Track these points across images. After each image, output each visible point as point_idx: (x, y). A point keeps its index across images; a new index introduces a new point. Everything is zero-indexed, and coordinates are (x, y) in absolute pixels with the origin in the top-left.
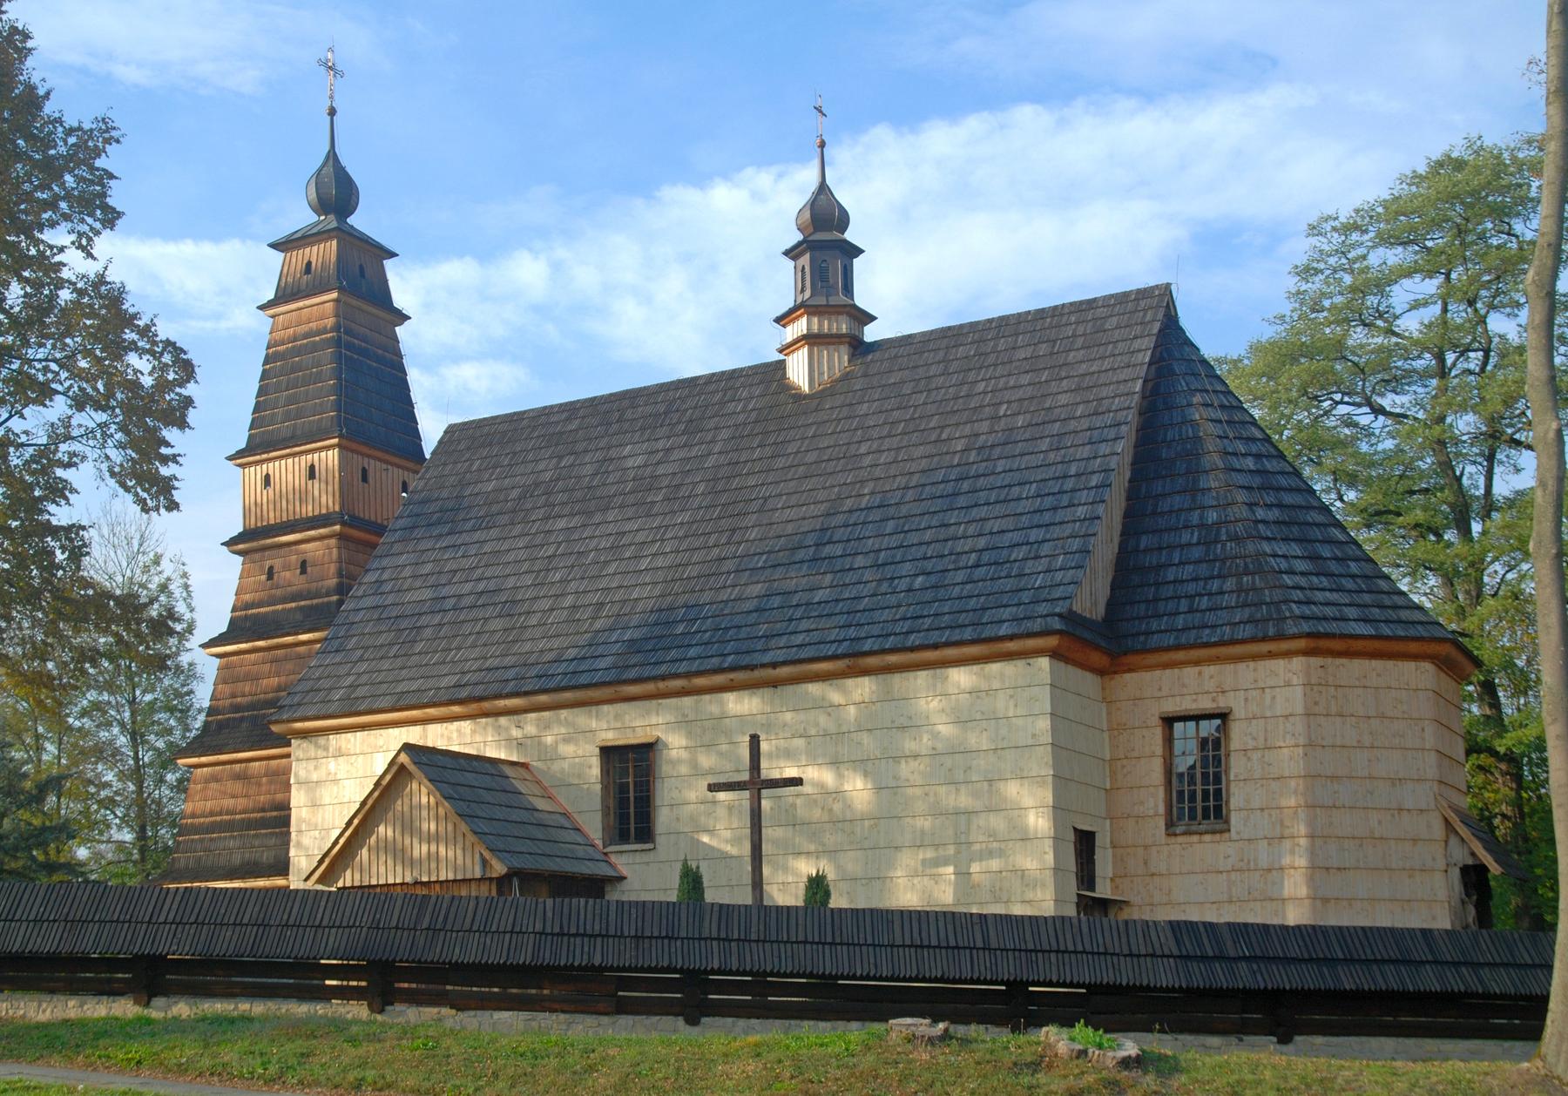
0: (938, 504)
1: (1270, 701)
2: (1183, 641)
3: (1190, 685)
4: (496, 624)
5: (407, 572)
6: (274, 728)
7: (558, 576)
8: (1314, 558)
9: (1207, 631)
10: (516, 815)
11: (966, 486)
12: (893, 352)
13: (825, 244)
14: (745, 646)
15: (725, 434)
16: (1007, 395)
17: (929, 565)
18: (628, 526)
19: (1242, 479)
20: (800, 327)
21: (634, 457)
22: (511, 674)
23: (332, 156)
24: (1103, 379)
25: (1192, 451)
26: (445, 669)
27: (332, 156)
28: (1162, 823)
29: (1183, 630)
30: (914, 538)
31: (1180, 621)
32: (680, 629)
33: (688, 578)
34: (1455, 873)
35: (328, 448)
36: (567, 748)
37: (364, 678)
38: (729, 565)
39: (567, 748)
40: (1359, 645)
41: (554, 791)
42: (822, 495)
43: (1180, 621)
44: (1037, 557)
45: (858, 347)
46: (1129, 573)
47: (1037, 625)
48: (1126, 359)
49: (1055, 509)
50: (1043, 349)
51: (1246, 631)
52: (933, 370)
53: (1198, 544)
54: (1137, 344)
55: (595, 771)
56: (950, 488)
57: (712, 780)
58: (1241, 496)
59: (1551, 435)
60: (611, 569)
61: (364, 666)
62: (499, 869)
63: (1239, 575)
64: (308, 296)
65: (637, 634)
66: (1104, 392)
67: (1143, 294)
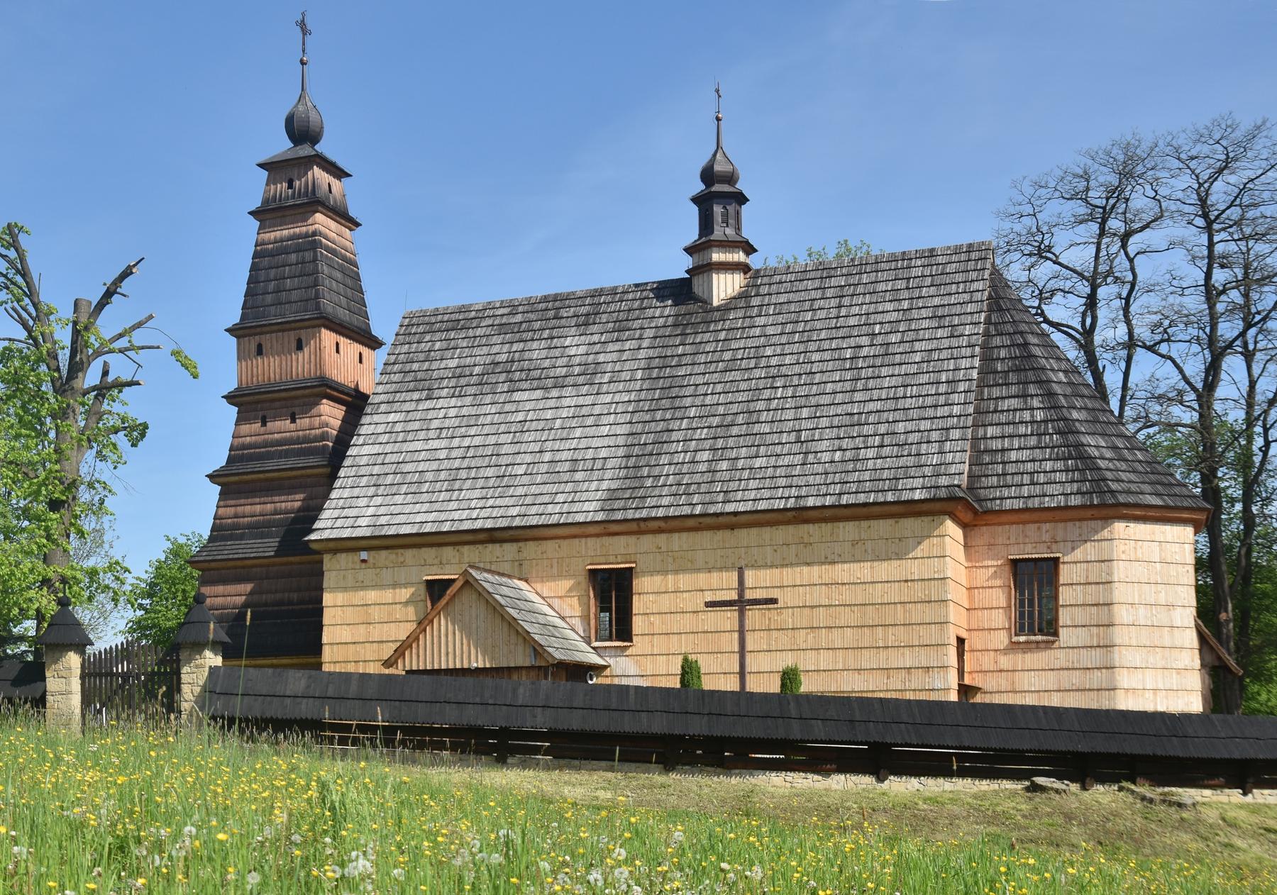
2: (1030, 505)
8: (1114, 448)
9: (1047, 499)
21: (575, 345)
29: (1029, 497)
33: (645, 444)
49: (936, 406)
53: (1032, 435)
54: (975, 286)
57: (709, 597)
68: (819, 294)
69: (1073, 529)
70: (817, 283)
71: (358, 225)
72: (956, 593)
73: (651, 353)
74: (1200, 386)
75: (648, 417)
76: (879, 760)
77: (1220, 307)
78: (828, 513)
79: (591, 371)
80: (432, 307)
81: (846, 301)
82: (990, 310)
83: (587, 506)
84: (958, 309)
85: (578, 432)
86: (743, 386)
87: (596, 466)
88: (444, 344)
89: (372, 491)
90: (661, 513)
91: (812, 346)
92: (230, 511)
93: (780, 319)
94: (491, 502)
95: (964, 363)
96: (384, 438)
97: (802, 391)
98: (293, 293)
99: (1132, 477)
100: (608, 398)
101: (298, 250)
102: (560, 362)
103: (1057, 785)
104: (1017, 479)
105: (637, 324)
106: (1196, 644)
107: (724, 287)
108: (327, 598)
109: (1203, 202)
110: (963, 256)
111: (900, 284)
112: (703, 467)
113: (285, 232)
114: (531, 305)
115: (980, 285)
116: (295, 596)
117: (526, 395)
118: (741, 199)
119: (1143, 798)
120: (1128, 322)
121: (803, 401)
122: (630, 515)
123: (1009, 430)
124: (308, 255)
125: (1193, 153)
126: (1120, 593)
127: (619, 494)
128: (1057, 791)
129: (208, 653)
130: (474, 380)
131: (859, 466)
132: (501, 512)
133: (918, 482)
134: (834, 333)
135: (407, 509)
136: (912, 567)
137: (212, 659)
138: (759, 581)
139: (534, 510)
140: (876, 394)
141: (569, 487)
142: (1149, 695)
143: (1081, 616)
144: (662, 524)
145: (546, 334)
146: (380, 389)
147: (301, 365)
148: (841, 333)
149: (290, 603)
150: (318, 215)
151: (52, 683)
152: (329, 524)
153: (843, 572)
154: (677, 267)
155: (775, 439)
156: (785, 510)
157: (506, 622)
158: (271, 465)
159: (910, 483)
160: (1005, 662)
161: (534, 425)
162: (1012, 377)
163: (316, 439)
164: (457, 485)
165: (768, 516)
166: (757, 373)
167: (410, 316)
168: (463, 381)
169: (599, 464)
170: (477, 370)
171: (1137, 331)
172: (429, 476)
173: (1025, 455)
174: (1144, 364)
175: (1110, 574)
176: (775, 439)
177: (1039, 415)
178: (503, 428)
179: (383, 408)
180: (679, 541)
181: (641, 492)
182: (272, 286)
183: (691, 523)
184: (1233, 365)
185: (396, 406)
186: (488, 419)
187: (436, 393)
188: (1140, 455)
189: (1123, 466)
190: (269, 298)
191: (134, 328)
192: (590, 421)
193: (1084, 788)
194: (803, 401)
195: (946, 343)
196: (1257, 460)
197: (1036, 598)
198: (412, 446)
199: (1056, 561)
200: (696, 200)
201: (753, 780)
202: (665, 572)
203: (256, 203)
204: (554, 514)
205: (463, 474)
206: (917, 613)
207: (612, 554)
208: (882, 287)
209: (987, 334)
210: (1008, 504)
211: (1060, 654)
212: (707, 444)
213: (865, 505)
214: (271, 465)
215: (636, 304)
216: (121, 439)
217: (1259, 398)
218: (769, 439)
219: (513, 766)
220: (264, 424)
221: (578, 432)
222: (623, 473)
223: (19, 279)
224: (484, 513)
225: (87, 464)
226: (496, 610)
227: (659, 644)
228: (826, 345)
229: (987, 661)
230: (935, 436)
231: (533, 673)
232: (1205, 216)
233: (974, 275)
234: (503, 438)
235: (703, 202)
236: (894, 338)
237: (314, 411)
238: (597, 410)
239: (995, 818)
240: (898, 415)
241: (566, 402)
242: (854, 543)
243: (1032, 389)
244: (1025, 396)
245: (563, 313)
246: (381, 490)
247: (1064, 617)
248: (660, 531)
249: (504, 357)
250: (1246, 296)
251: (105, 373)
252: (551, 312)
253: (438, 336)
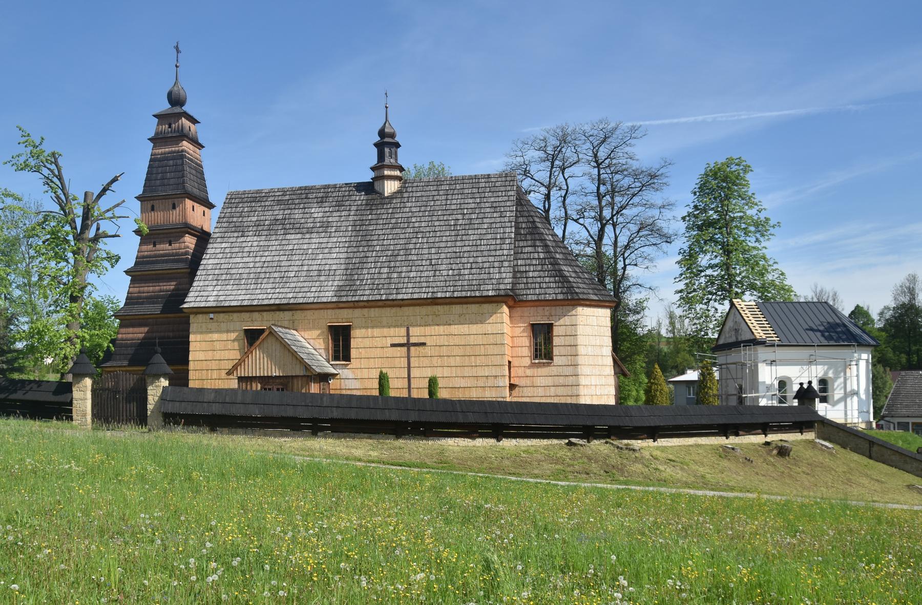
8: (575, 272)
21: (317, 212)
32: (358, 283)
54: (510, 193)
68: (436, 193)
69: (559, 310)
70: (435, 188)
71: (203, 147)
72: (507, 340)
73: (355, 218)
74: (596, 239)
75: (355, 250)
76: (498, 431)
77: (604, 203)
78: (447, 301)
79: (326, 226)
80: (242, 190)
81: (450, 197)
82: (517, 205)
83: (327, 294)
84: (503, 204)
85: (321, 256)
86: (402, 236)
87: (331, 273)
88: (249, 209)
89: (215, 283)
90: (365, 298)
91: (435, 218)
92: (136, 290)
93: (418, 204)
94: (278, 290)
95: (508, 230)
96: (220, 256)
97: (431, 240)
98: (171, 178)
99: (584, 286)
100: (335, 239)
101: (173, 159)
102: (309, 220)
103: (581, 442)
104: (533, 285)
105: (347, 203)
106: (612, 363)
107: (390, 187)
108: (192, 337)
109: (596, 156)
110: (504, 179)
111: (475, 190)
112: (385, 276)
113: (167, 150)
114: (293, 191)
115: (512, 193)
116: (171, 334)
117: (293, 237)
118: (397, 145)
119: (618, 447)
120: (565, 208)
121: (432, 245)
122: (350, 299)
123: (528, 262)
124: (179, 162)
125: (591, 133)
126: (581, 340)
127: (343, 288)
128: (581, 445)
129: (162, 380)
130: (266, 228)
131: (461, 278)
132: (283, 296)
133: (490, 287)
134: (445, 212)
135: (234, 293)
136: (488, 328)
137: (164, 383)
138: (417, 333)
139: (300, 295)
140: (467, 243)
141: (317, 284)
142: (593, 388)
143: (563, 351)
144: (366, 304)
145: (302, 206)
146: (217, 230)
147: (174, 217)
148: (448, 212)
149: (168, 338)
150: (184, 142)
151: (76, 394)
152: (193, 299)
153: (455, 329)
154: (367, 176)
155: (419, 263)
156: (427, 298)
157: (289, 352)
158: (158, 267)
159: (487, 287)
160: (529, 372)
161: (298, 252)
162: (529, 237)
163: (183, 254)
164: (260, 281)
165: (418, 301)
166: (409, 230)
167: (231, 194)
168: (260, 228)
169: (332, 273)
170: (267, 223)
171: (569, 212)
172: (245, 276)
173: (536, 274)
174: (572, 227)
175: (576, 331)
176: (419, 263)
177: (542, 255)
178: (282, 253)
179: (219, 240)
180: (374, 312)
181: (354, 288)
182: (159, 176)
183: (380, 303)
184: (609, 229)
185: (226, 240)
186: (274, 248)
187: (246, 234)
188: (586, 276)
189: (579, 280)
190: (158, 182)
191: (115, 207)
192: (326, 251)
193: (589, 442)
194: (432, 245)
195: (498, 220)
196: (620, 273)
197: (543, 343)
198: (235, 260)
199: (550, 326)
200: (376, 145)
201: (439, 442)
202: (367, 327)
203: (152, 134)
204: (311, 297)
205: (262, 276)
206: (491, 350)
207: (341, 318)
208: (466, 191)
209: (516, 216)
210: (530, 298)
211: (554, 368)
212: (386, 264)
213: (466, 297)
214: (158, 267)
215: (347, 193)
216: (106, 264)
217: (619, 244)
218: (417, 263)
219: (320, 437)
220: (155, 245)
221: (321, 256)
222: (344, 278)
223: (55, 180)
224: (275, 296)
225: (91, 278)
226: (286, 347)
227: (364, 364)
228: (441, 218)
229: (520, 372)
230: (496, 264)
231: (304, 379)
232: (596, 162)
233: (509, 188)
234: (282, 258)
235: (380, 146)
236: (473, 216)
237: (181, 240)
238: (330, 245)
239: (557, 461)
240: (479, 254)
241: (314, 241)
242: (460, 315)
243: (538, 243)
244: (535, 246)
245: (310, 196)
246: (220, 283)
247: (556, 351)
248: (365, 307)
249: (280, 217)
250: (612, 198)
251: (98, 229)
252: (303, 195)
253: (246, 205)
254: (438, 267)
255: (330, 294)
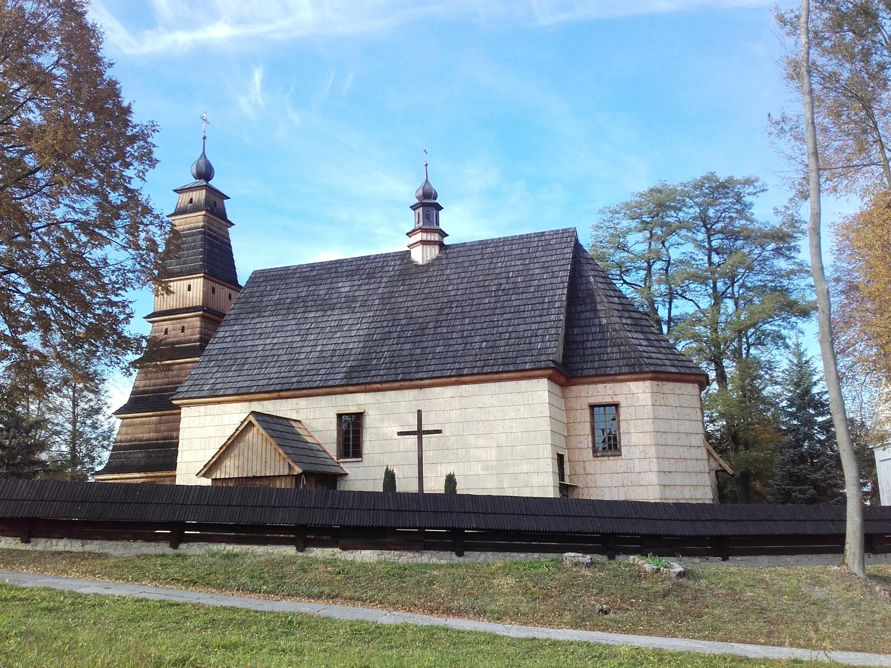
0: (491, 312)
1: (636, 397)
3: (602, 392)
4: (284, 358)
5: (238, 333)
6: (175, 402)
7: (312, 337)
8: (648, 340)
10: (301, 445)
11: (499, 305)
12: (458, 249)
13: (428, 205)
14: (406, 370)
15: (385, 280)
16: (512, 269)
17: (488, 338)
18: (344, 317)
19: (615, 307)
20: (419, 237)
21: (344, 287)
22: (295, 380)
23: (204, 155)
24: (553, 264)
25: (591, 295)
26: (261, 377)
27: (204, 155)
28: (591, 451)
30: (478, 326)
31: (596, 365)
32: (374, 362)
34: (713, 473)
35: (198, 278)
36: (317, 417)
37: (219, 380)
38: (395, 335)
39: (317, 417)
40: (672, 376)
41: (313, 434)
42: (433, 307)
43: (596, 365)
44: (536, 336)
45: (442, 246)
46: (571, 343)
47: (543, 365)
48: (562, 256)
49: (541, 316)
50: (525, 251)
51: (626, 369)
52: (477, 257)
54: (566, 250)
55: (334, 426)
56: (492, 306)
58: (616, 313)
59: (825, 291)
60: (338, 335)
61: (219, 375)
62: (298, 470)
63: (619, 346)
64: (190, 212)
65: (354, 364)
66: (555, 269)
67: (565, 231)
95: (559, 292)
118: (153, 163)
240: (521, 321)
254: (470, 340)
255: (342, 375)
